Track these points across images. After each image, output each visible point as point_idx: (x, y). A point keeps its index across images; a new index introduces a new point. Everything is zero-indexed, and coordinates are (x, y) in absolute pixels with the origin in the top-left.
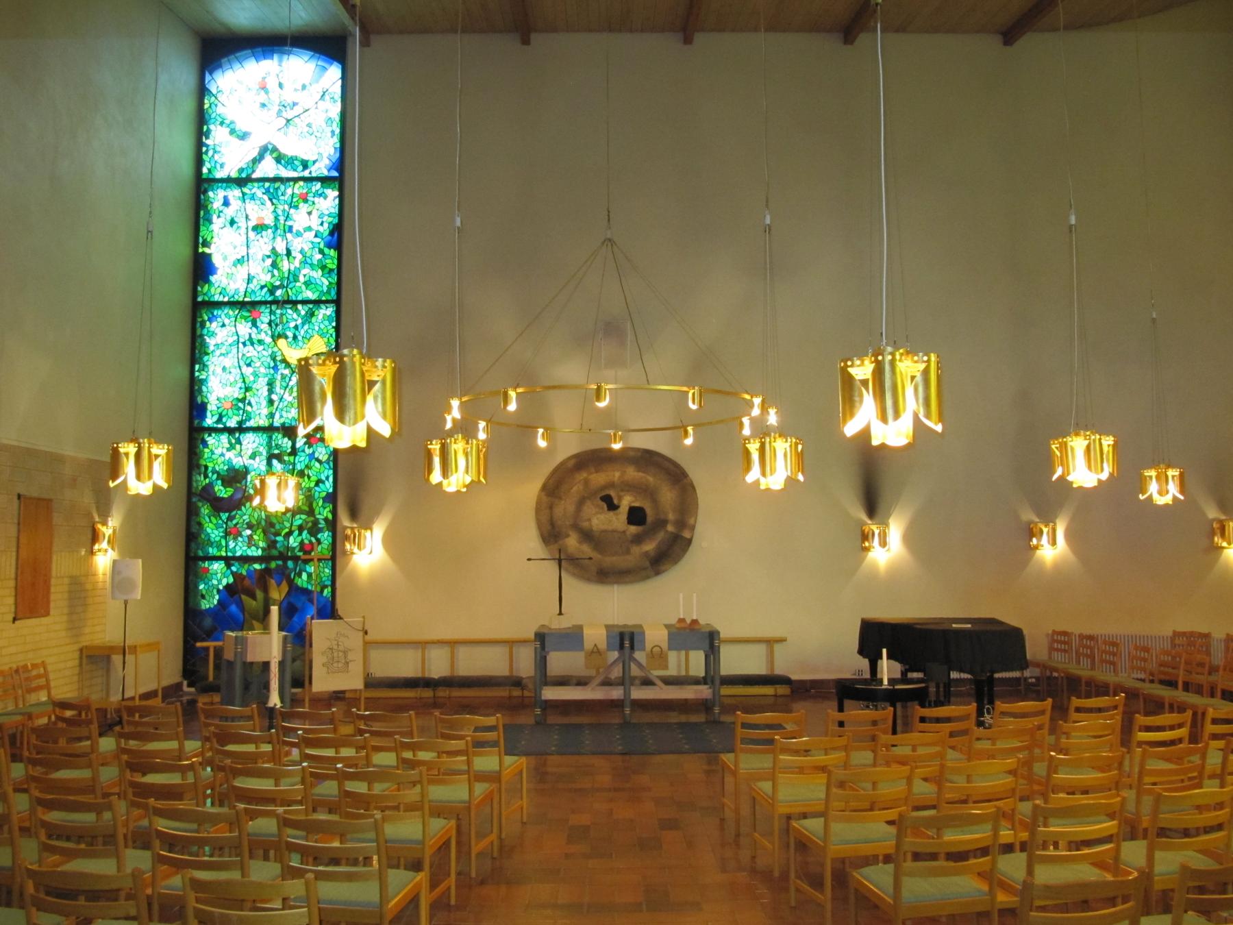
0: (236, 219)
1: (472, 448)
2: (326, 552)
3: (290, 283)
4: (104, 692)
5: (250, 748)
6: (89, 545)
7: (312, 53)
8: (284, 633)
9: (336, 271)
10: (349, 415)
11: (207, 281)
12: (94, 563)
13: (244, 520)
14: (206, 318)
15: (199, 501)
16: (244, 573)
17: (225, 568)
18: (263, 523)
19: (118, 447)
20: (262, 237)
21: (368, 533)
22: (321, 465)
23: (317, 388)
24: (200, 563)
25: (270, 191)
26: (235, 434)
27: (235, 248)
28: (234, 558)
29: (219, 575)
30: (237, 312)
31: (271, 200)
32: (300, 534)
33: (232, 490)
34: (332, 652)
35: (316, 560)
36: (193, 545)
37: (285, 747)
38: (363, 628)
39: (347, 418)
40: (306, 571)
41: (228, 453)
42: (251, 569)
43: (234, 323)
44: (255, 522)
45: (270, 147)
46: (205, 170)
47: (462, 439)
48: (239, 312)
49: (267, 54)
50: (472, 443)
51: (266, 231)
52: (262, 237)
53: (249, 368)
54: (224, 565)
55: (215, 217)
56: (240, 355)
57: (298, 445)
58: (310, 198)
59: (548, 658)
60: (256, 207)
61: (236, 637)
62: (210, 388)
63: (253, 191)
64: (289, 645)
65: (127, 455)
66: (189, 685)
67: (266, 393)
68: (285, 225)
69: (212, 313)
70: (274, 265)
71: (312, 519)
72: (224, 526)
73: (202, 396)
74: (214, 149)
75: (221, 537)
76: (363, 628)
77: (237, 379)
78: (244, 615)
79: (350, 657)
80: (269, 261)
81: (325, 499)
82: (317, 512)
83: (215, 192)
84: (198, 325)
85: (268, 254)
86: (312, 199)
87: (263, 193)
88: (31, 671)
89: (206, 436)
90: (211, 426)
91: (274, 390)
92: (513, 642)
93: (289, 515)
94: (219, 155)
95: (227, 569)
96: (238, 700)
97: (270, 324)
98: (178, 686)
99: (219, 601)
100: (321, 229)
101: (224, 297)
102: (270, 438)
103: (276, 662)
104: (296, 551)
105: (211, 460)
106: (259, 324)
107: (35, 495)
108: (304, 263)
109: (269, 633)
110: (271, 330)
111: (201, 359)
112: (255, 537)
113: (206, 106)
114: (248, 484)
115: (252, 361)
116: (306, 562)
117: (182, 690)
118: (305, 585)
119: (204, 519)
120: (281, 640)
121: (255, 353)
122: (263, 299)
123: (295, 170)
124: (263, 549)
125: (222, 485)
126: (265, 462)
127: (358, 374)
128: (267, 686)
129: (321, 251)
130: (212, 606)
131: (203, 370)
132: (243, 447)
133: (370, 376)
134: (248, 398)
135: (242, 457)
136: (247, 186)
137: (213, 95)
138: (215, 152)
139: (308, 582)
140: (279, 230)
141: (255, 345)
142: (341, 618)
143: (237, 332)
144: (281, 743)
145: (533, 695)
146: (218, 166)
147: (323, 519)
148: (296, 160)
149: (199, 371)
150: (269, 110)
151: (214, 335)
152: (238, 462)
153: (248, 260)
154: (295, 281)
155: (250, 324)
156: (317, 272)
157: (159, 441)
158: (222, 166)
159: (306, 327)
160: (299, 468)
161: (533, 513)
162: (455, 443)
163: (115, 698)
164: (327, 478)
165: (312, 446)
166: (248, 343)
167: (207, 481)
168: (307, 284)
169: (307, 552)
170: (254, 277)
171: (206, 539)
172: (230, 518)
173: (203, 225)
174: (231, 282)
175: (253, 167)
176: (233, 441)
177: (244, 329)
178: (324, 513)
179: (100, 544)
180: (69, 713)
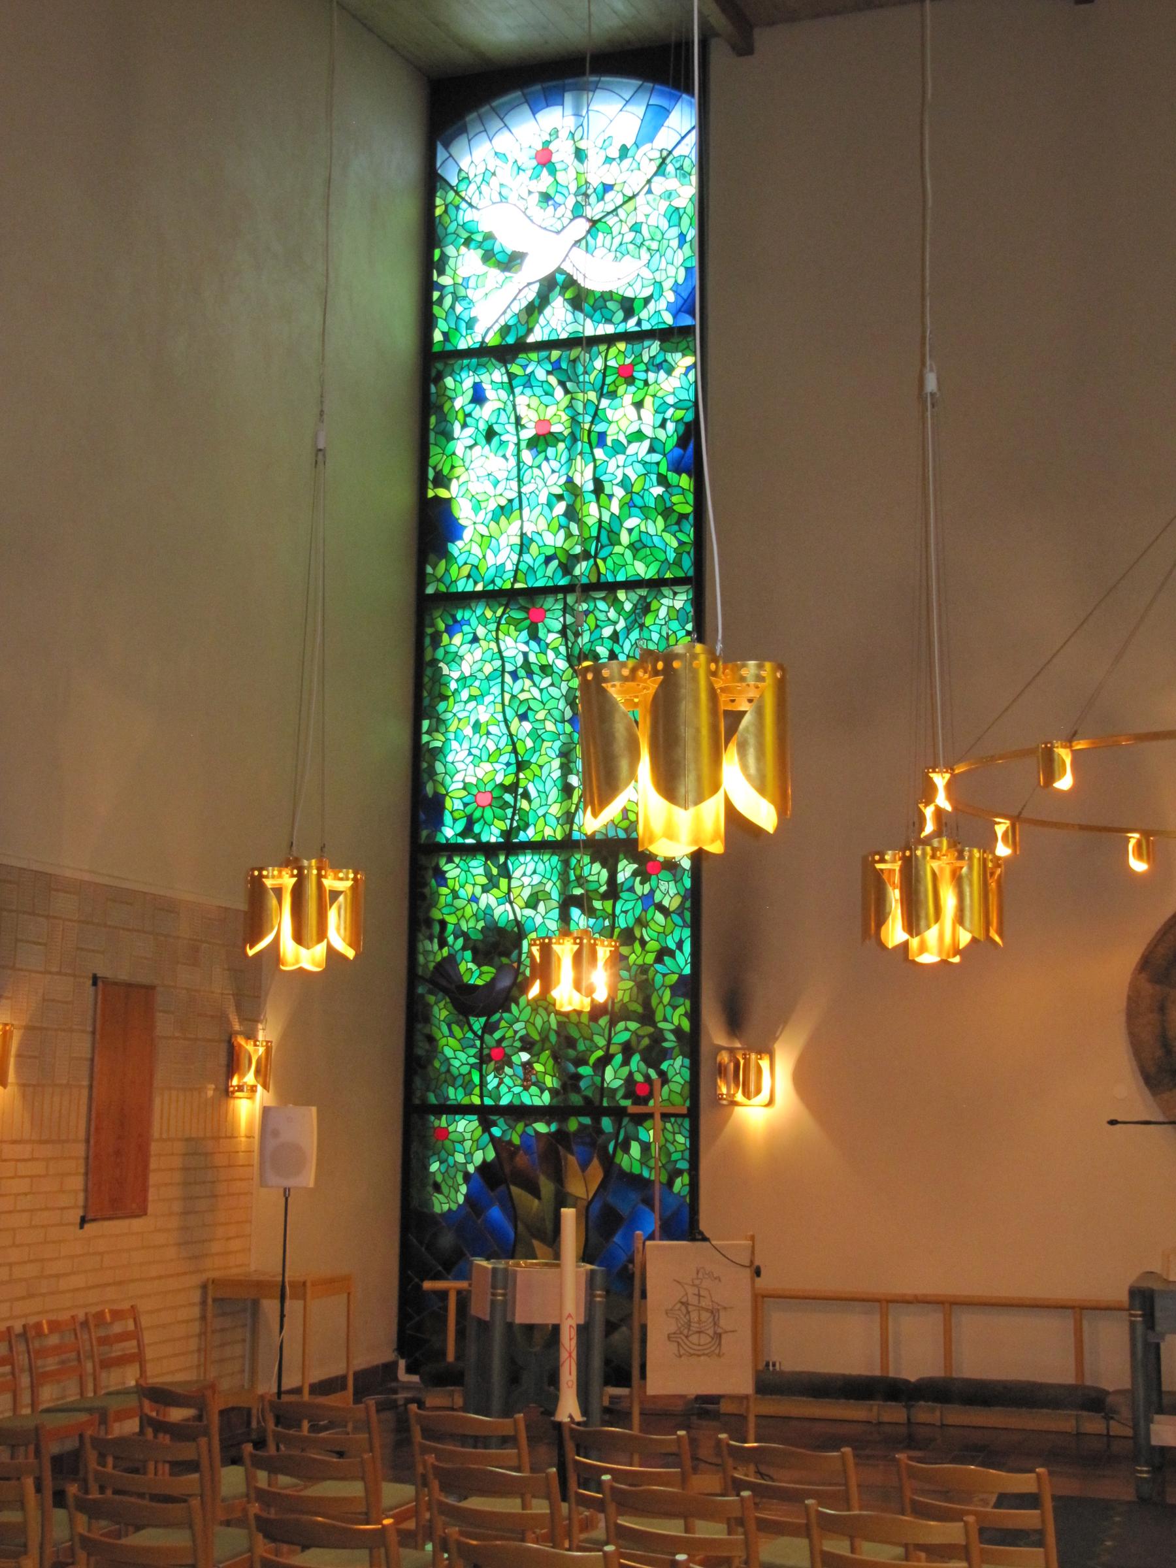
0: (496, 428)
1: (970, 868)
2: (677, 1100)
3: (602, 547)
4: (247, 1375)
5: (509, 1506)
6: (222, 1078)
7: (640, 83)
8: (589, 1267)
9: (691, 518)
10: (688, 784)
11: (445, 554)
12: (231, 1109)
13: (516, 1032)
14: (442, 626)
15: (431, 992)
16: (516, 1140)
17: (480, 1129)
18: (553, 1038)
19: (261, 876)
20: (547, 459)
21: (765, 1063)
22: (666, 918)
23: (620, 729)
24: (432, 1118)
25: (560, 368)
26: (497, 857)
27: (496, 483)
28: (498, 1110)
29: (468, 1144)
30: (500, 612)
31: (562, 384)
32: (626, 1062)
33: (493, 970)
34: (688, 1312)
35: (657, 1116)
36: (418, 1082)
37: (581, 1509)
38: (752, 1262)
39: (682, 790)
40: (637, 1139)
41: (485, 895)
42: (530, 1131)
43: (494, 633)
44: (536, 1037)
45: (560, 278)
46: (437, 336)
47: (949, 847)
48: (504, 613)
49: (552, 97)
50: (971, 858)
51: (555, 446)
52: (547, 459)
53: (525, 724)
54: (476, 1123)
55: (457, 427)
56: (507, 697)
57: (621, 878)
58: (639, 375)
59: (1163, 1346)
60: (535, 402)
61: (494, 1270)
62: (449, 766)
63: (528, 371)
64: (599, 1292)
65: (278, 891)
66: (410, 1370)
67: (557, 774)
68: (590, 432)
69: (454, 617)
70: (571, 514)
71: (650, 1030)
72: (478, 1043)
73: (435, 781)
74: (454, 293)
75: (472, 1066)
76: (752, 1262)
77: (501, 746)
78: (516, 1227)
79: (724, 1322)
80: (561, 507)
81: (674, 988)
82: (659, 1016)
83: (458, 378)
84: (427, 641)
85: (559, 491)
86: (642, 376)
87: (549, 373)
88: (112, 1323)
89: (443, 861)
90: (452, 841)
91: (572, 765)
92: (1083, 1308)
93: (603, 1021)
94: (465, 303)
95: (484, 1131)
96: (496, 1403)
97: (563, 632)
98: (389, 1369)
99: (467, 1197)
100: (661, 435)
101: (476, 583)
102: (566, 863)
103: (571, 1326)
104: (618, 1098)
105: (453, 910)
106: (541, 634)
107: (123, 976)
108: (629, 505)
109: (558, 1266)
110: (566, 645)
111: (434, 708)
112: (538, 1067)
113: (438, 212)
114: (524, 956)
115: (529, 708)
116: (640, 1119)
117: (396, 1379)
118: (636, 1169)
119: (440, 1029)
120: (583, 1280)
121: (536, 692)
122: (550, 584)
123: (609, 321)
124: (554, 1092)
125: (473, 961)
126: (555, 914)
127: (704, 696)
128: (554, 1379)
129: (662, 480)
130: (454, 1207)
131: (437, 731)
132: (514, 883)
133: (733, 701)
134: (522, 783)
135: (511, 903)
136: (518, 361)
137: (452, 188)
138: (456, 298)
139: (643, 1162)
140: (579, 443)
141: (535, 677)
142: (705, 1239)
143: (500, 652)
144: (573, 1499)
145: (1129, 1432)
146: (463, 326)
147: (672, 1031)
148: (612, 299)
149: (429, 732)
150: (557, 206)
151: (457, 659)
152: (503, 914)
153: (521, 508)
154: (612, 544)
155: (524, 635)
156: (654, 522)
157: (337, 866)
158: (471, 323)
159: (635, 635)
160: (623, 925)
161: (1122, 1018)
162: (933, 857)
163: (267, 1387)
164: (680, 945)
165: (649, 880)
166: (521, 673)
167: (445, 951)
168: (635, 548)
169: (641, 1100)
170: (532, 540)
171: (443, 1069)
172: (489, 1028)
173: (436, 444)
174: (489, 555)
175: (527, 322)
176: (495, 871)
177: (514, 645)
178: (676, 1018)
179: (242, 1076)
180: (177, 1415)
